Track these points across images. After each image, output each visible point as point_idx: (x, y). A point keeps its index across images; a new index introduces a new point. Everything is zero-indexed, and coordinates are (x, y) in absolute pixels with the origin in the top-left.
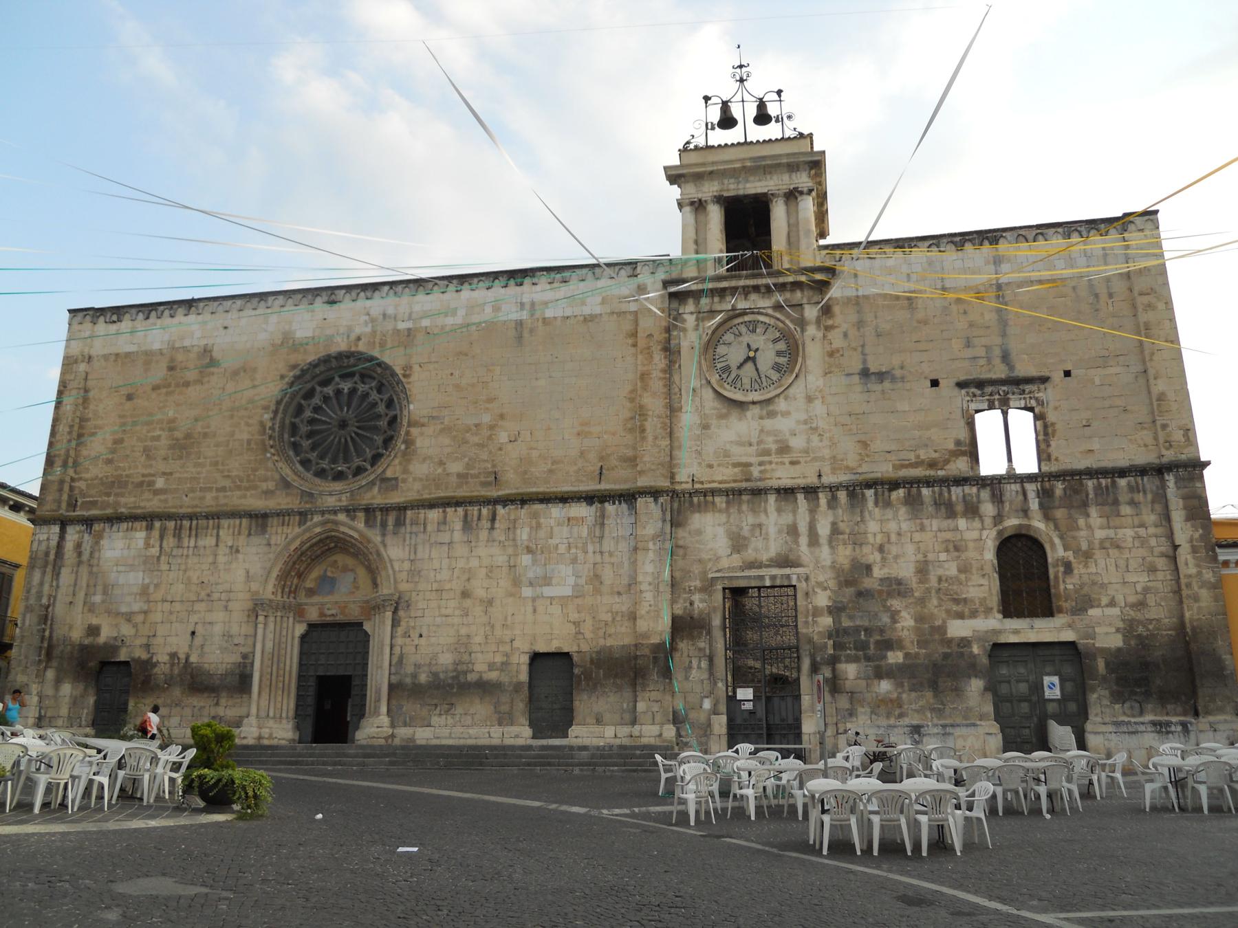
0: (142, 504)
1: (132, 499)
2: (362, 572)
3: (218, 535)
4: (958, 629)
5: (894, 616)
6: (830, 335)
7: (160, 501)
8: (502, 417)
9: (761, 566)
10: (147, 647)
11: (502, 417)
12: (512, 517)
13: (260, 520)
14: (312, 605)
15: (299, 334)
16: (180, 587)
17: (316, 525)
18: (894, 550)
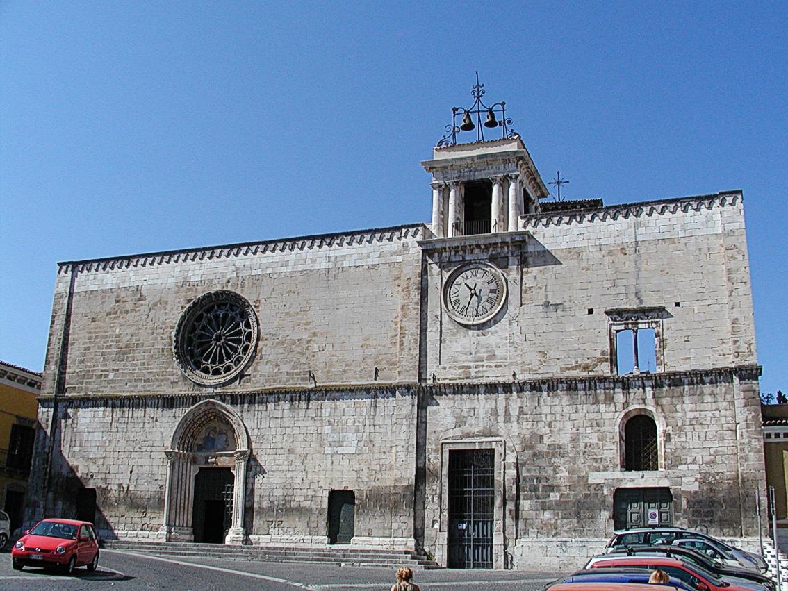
0: (101, 390)
4: (595, 478)
13: (169, 402)
18: (558, 425)
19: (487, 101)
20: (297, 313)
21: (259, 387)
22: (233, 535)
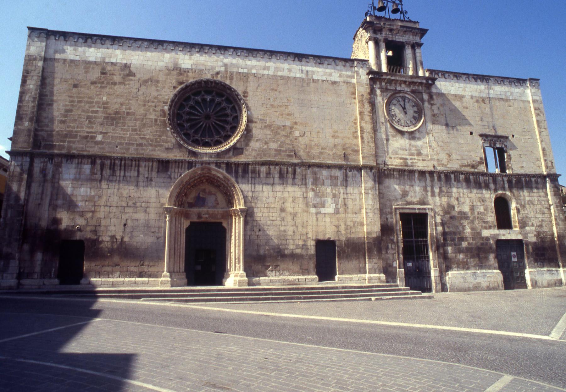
0: (88, 149)
1: (81, 146)
3: (138, 171)
4: (486, 233)
5: (464, 227)
6: (433, 107)
7: (100, 148)
8: (296, 123)
9: (413, 203)
10: (95, 232)
11: (296, 123)
12: (304, 173)
13: (164, 166)
15: (183, 66)
16: (116, 198)
17: (197, 170)
18: (462, 200)
20: (280, 106)
21: (250, 159)
22: (235, 278)
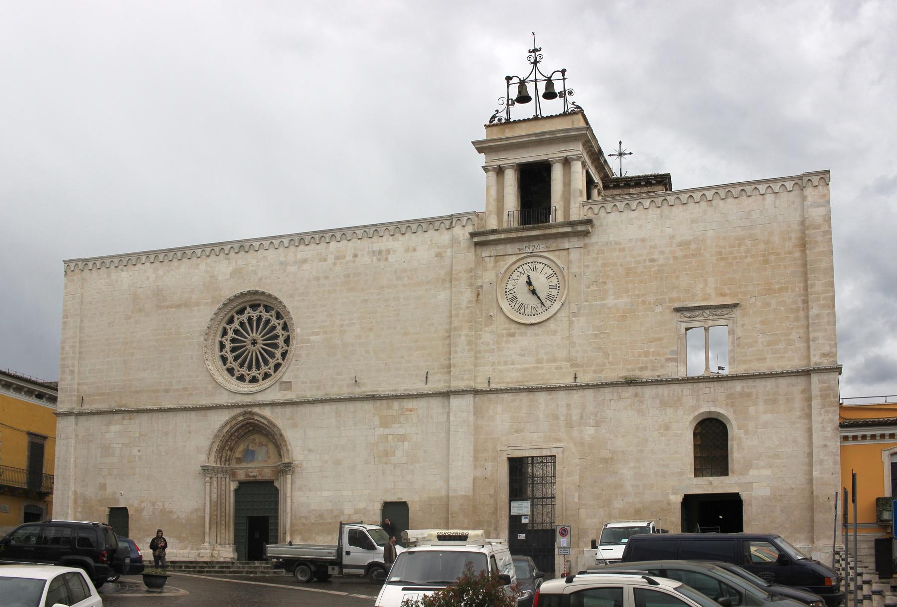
2: (271, 447)
14: (241, 469)
19: (547, 67)
